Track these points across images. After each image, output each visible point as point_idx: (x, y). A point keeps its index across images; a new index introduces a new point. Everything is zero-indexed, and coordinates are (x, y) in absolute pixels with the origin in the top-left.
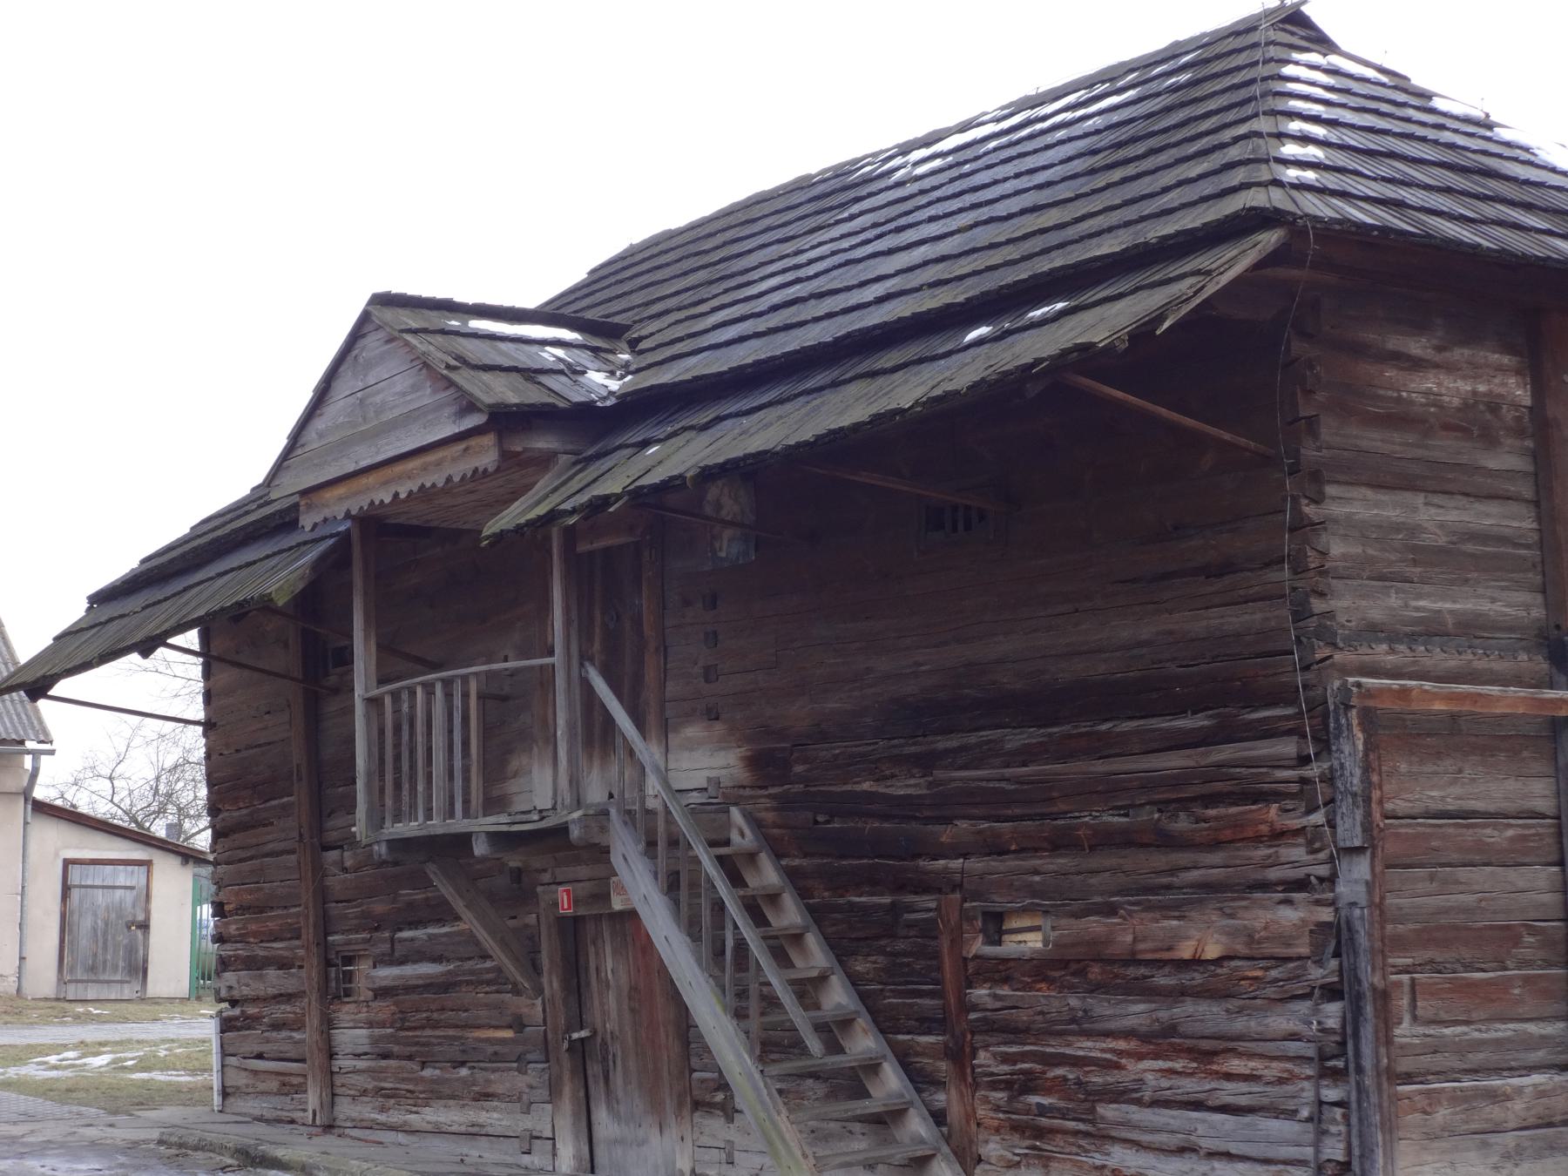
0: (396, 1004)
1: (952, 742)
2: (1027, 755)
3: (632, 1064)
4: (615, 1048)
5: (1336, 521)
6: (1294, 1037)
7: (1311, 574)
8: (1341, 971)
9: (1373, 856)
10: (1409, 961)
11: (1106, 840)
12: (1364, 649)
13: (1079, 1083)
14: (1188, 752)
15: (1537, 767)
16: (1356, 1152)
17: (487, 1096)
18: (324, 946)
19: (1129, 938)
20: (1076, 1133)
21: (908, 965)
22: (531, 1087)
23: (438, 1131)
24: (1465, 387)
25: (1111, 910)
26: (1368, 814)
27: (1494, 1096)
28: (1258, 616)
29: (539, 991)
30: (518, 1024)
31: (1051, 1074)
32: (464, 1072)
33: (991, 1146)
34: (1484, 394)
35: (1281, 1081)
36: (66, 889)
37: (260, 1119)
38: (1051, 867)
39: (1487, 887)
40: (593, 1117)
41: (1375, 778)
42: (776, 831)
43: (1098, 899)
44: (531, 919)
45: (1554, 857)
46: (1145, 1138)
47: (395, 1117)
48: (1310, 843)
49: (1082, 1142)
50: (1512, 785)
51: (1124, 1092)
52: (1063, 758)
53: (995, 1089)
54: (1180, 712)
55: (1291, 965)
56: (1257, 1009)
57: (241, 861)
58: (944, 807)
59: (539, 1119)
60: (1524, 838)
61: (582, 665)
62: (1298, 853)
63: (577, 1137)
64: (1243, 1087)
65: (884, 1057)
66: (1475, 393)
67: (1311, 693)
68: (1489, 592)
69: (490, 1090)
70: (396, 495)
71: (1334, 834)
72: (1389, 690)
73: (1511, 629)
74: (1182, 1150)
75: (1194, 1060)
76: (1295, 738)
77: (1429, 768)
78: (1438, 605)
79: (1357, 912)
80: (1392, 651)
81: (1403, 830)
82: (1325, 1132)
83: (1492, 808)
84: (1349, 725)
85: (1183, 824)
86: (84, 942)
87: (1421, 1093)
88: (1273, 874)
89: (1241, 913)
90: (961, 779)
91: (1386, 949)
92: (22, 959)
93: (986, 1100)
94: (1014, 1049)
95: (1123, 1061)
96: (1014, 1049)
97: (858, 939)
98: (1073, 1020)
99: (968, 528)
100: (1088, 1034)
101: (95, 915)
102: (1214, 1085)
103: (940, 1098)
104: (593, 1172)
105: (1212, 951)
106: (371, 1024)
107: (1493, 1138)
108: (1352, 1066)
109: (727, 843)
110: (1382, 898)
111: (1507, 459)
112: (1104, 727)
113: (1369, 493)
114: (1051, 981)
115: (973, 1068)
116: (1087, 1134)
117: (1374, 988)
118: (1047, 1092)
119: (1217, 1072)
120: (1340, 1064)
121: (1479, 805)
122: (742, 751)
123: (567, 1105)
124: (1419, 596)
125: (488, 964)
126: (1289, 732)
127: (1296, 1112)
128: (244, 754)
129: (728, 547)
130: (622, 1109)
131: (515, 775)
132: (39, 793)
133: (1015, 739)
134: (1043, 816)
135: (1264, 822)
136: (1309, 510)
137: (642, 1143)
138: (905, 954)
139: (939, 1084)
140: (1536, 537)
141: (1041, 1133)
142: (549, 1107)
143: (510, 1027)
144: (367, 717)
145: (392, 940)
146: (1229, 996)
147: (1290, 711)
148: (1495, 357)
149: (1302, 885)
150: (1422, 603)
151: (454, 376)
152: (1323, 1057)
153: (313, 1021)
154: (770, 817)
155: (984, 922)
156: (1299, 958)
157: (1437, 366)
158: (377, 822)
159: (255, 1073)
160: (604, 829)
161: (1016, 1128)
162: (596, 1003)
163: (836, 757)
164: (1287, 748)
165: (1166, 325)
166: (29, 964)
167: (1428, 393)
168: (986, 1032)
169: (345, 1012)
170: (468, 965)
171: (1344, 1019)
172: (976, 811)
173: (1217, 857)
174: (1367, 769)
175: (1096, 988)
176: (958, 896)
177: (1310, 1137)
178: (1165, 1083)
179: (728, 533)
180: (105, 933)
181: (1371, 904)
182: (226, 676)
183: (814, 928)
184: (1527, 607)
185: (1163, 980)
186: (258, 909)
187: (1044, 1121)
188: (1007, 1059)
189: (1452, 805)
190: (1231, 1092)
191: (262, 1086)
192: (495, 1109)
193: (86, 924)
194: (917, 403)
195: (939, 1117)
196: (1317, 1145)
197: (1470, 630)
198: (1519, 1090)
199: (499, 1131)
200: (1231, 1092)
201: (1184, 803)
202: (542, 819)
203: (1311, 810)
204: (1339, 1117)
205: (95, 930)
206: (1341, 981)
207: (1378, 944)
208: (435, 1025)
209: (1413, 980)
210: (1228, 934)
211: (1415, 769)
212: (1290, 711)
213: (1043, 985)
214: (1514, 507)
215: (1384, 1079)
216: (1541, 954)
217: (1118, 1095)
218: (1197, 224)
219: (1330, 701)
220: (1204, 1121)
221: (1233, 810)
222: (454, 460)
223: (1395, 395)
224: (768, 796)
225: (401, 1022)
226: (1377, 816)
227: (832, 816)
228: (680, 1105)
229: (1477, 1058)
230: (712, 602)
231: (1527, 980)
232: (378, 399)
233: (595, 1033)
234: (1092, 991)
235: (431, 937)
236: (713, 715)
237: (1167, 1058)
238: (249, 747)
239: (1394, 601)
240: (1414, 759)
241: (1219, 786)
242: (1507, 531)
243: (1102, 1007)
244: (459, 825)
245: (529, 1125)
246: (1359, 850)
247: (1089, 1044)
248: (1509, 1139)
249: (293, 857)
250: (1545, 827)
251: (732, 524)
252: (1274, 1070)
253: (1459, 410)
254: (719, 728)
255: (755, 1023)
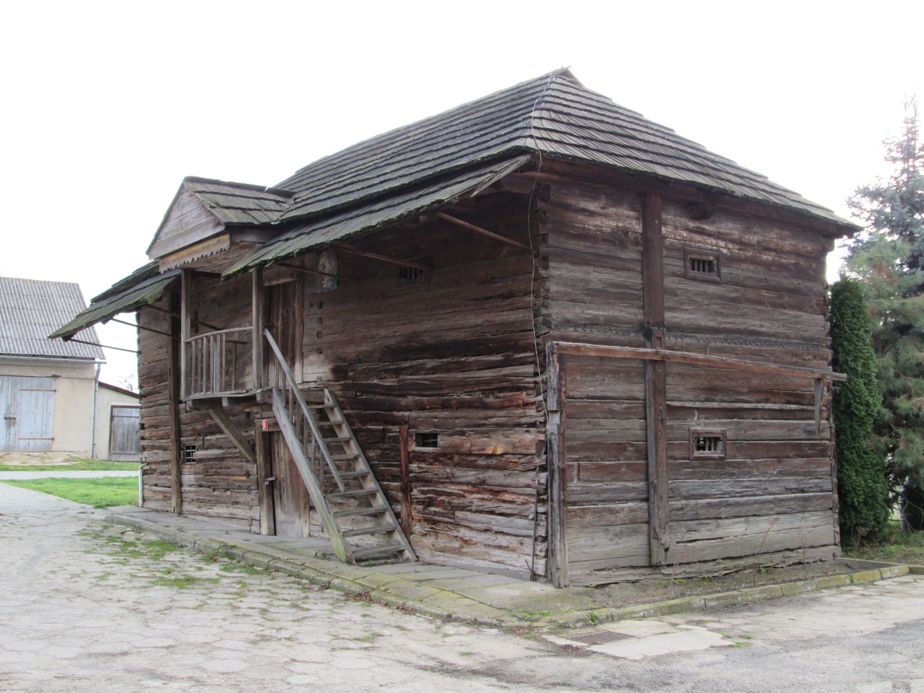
0: (204, 465)
1: (407, 364)
2: (434, 370)
3: (289, 491)
4: (284, 485)
5: (553, 277)
6: (528, 486)
7: (541, 298)
8: (547, 460)
9: (561, 414)
10: (577, 456)
11: (463, 405)
12: (563, 330)
13: (449, 503)
14: (493, 370)
15: (636, 379)
16: (550, 533)
17: (237, 503)
18: (178, 442)
19: (469, 445)
20: (448, 523)
21: (389, 454)
22: (252, 500)
23: (219, 516)
24: (613, 224)
25: (463, 433)
26: (560, 397)
27: (612, 511)
28: (521, 315)
29: (255, 461)
30: (248, 474)
31: (439, 499)
32: (228, 493)
33: (417, 527)
34: (621, 227)
35: (523, 504)
36: (112, 417)
37: (157, 511)
38: (442, 416)
39: (612, 427)
40: (276, 512)
41: (563, 383)
42: (341, 399)
43: (458, 429)
44: (253, 433)
45: (642, 416)
46: (472, 525)
47: (204, 510)
48: (537, 408)
49: (450, 526)
50: (626, 387)
51: (465, 507)
52: (448, 371)
53: (419, 504)
54: (490, 353)
55: (529, 457)
56: (515, 474)
57: (150, 407)
58: (403, 390)
59: (255, 513)
60: (630, 408)
61: (264, 330)
62: (532, 412)
63: (269, 520)
64: (509, 506)
65: (378, 491)
66: (617, 226)
67: (540, 347)
68: (619, 308)
69: (238, 500)
70: (193, 259)
71: (546, 405)
72: (571, 347)
73: (628, 323)
74: (486, 530)
75: (491, 494)
76: (533, 365)
77: (590, 379)
78: (597, 313)
79: (554, 437)
80: (576, 331)
81: (577, 404)
82: (539, 525)
83: (616, 395)
84: (553, 361)
85: (490, 399)
86: (119, 439)
87: (579, 509)
88: (523, 420)
89: (511, 436)
90: (410, 379)
91: (565, 452)
92: (94, 444)
93: (415, 509)
94: (426, 489)
95: (466, 494)
96: (426, 489)
97: (370, 443)
98: (448, 478)
99: (416, 277)
100: (453, 483)
101: (124, 428)
102: (498, 505)
103: (398, 508)
104: (275, 534)
105: (499, 451)
106: (196, 473)
107: (610, 528)
108: (549, 499)
109: (323, 403)
110: (564, 431)
111: (631, 254)
112: (463, 359)
113: (569, 266)
114: (440, 462)
115: (411, 496)
116: (452, 523)
117: (559, 467)
118: (438, 506)
119: (500, 500)
120: (545, 497)
121: (611, 394)
122: (331, 366)
123: (265, 507)
124: (589, 309)
125: (237, 450)
126: (531, 363)
127: (528, 516)
128: (151, 365)
129: (327, 283)
130: (286, 509)
131: (248, 374)
132: (101, 379)
133: (430, 363)
134: (439, 395)
135: (520, 399)
136: (542, 272)
137: (293, 522)
138: (387, 449)
139: (398, 502)
140: (641, 286)
141: (435, 522)
142: (258, 508)
143: (244, 475)
144: (186, 349)
145: (203, 440)
146: (506, 469)
147: (532, 354)
148: (627, 212)
149: (533, 425)
150: (590, 312)
151: (213, 211)
152: (539, 494)
153: (174, 471)
154: (339, 393)
155: (416, 437)
156: (532, 454)
157: (601, 215)
158: (188, 393)
159: (154, 491)
160: (270, 397)
161: (426, 520)
162: (277, 466)
163: (364, 369)
164: (530, 369)
165: (475, 193)
166: (96, 446)
167: (596, 226)
168: (416, 481)
169: (187, 468)
170: (230, 450)
171: (547, 479)
172: (414, 392)
173: (503, 413)
174: (560, 378)
175: (456, 465)
176: (406, 426)
177: (533, 526)
178: (480, 503)
179: (327, 278)
180: (128, 435)
181: (559, 433)
182: (145, 333)
183: (354, 438)
184: (636, 315)
185: (481, 462)
186: (156, 426)
187: (436, 518)
188: (423, 492)
189: (599, 394)
190: (505, 508)
191: (157, 497)
192: (239, 508)
193: (120, 432)
194: (378, 224)
195: (397, 515)
196: (535, 530)
197: (610, 323)
198: (622, 509)
199: (241, 517)
200: (505, 508)
201: (492, 391)
202: (247, 392)
203: (538, 394)
204: (544, 519)
205: (123, 433)
206: (547, 464)
207: (561, 450)
208: (218, 474)
209: (579, 464)
210: (505, 444)
211: (584, 379)
212: (532, 354)
213: (437, 463)
214: (631, 274)
215: (562, 504)
216: (635, 455)
217: (463, 508)
218: (496, 153)
219: (547, 350)
220: (494, 519)
221: (509, 394)
222: (214, 245)
223: (582, 226)
224: (339, 385)
225: (206, 473)
226: (563, 397)
227: (363, 393)
228: (305, 508)
229: (604, 496)
230: (321, 306)
231: (628, 465)
232: (186, 220)
233: (277, 478)
234: (455, 466)
235: (217, 439)
236: (320, 351)
237: (482, 493)
238: (153, 362)
239: (578, 310)
240: (584, 375)
241: (504, 384)
242: (628, 284)
243: (458, 472)
244: (217, 394)
245: (251, 515)
246: (556, 412)
247: (453, 487)
248: (617, 529)
249: (167, 406)
250: (639, 404)
251: (328, 274)
252: (521, 499)
253: (610, 233)
254: (322, 357)
255: (321, 477)
